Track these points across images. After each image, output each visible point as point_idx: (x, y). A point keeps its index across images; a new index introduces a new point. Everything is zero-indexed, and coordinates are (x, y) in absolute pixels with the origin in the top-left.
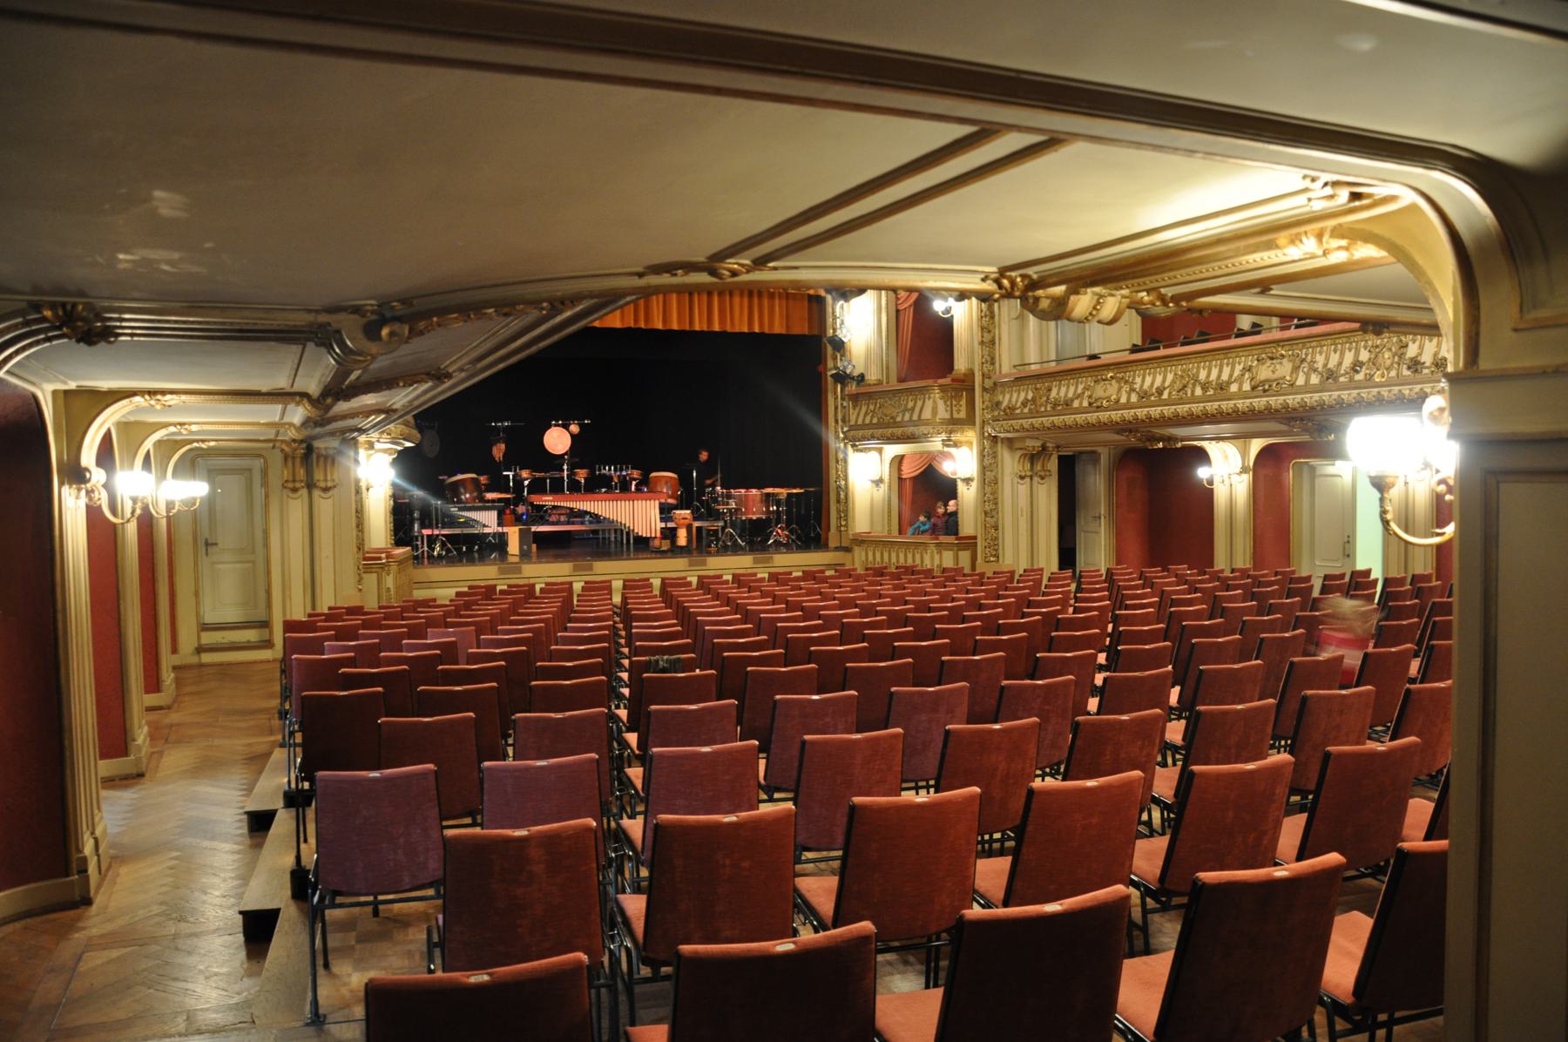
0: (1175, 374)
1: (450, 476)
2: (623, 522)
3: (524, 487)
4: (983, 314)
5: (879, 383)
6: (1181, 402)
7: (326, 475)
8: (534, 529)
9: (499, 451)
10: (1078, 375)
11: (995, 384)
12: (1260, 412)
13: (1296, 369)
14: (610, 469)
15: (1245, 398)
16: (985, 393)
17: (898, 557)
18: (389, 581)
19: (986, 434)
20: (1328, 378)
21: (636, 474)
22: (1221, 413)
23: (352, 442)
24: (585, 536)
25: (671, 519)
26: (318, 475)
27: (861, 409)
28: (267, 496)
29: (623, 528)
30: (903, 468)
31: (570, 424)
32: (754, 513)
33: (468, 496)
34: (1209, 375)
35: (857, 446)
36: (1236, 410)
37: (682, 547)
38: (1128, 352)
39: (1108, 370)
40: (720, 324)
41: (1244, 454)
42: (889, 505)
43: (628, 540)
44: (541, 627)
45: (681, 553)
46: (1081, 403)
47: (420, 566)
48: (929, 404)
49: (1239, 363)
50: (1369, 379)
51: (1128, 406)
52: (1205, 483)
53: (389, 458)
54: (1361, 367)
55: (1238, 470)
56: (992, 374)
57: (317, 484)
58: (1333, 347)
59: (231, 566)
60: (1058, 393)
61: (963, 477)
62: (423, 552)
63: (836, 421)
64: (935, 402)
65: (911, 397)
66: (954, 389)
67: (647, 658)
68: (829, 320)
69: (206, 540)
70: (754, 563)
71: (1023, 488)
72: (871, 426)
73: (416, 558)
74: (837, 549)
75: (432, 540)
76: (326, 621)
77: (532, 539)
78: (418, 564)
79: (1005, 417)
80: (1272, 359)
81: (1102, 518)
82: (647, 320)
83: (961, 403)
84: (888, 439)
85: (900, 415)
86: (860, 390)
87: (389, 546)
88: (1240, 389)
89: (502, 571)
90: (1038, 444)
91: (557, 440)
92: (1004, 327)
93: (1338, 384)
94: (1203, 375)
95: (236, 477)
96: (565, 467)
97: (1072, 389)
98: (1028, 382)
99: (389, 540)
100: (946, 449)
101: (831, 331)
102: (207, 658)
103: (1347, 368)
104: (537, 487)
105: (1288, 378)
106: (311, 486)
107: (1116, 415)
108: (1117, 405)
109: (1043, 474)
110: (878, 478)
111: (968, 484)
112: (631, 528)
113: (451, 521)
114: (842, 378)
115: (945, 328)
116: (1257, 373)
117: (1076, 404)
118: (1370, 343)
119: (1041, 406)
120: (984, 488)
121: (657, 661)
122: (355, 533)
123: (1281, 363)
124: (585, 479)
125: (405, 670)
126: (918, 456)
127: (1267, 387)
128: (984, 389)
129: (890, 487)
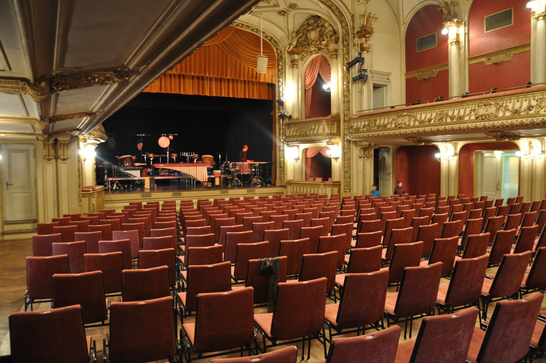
0: (437, 113)
1: (120, 156)
2: (192, 175)
3: (150, 161)
4: (344, 90)
5: (298, 119)
6: (440, 124)
7: (64, 152)
8: (156, 178)
9: (140, 146)
10: (389, 114)
11: (350, 119)
12: (480, 128)
13: (498, 110)
14: (186, 154)
15: (472, 123)
16: (345, 123)
17: (307, 190)
18: (94, 201)
19: (346, 139)
20: (515, 113)
21: (196, 156)
22: (460, 129)
23: (76, 138)
24: (175, 181)
25: (212, 174)
26: (60, 153)
27: (291, 130)
28: (36, 162)
29: (192, 178)
30: (307, 154)
31: (169, 136)
32: (246, 172)
33: (127, 164)
34: (453, 113)
35: (289, 144)
36: (468, 128)
37: (217, 186)
38: (405, 106)
39: (404, 112)
40: (232, 94)
41: (455, 147)
42: (302, 169)
43: (193, 182)
44: (173, 229)
45: (217, 188)
46: (391, 126)
47: (108, 194)
48: (321, 127)
49: (469, 108)
50: (537, 113)
51: (414, 127)
52: (438, 160)
53: (94, 147)
54: (533, 108)
55: (453, 154)
56: (348, 115)
57: (60, 157)
58: (517, 100)
59: (19, 195)
60: (380, 122)
61: (335, 157)
62: (109, 187)
63: (280, 135)
64: (324, 126)
65: (313, 124)
66: (332, 121)
67: (259, 260)
68: (277, 94)
69: (7, 182)
70: (247, 192)
71: (361, 162)
72: (296, 136)
73: (106, 190)
74: (280, 186)
75: (112, 183)
76: (60, 225)
77: (154, 182)
78: (107, 193)
79: (356, 132)
80: (485, 105)
81: (391, 174)
82: (203, 92)
83: (334, 127)
84: (304, 141)
85: (309, 132)
86: (290, 121)
87: (94, 185)
88: (470, 118)
89: (143, 196)
90: (367, 143)
91: (164, 142)
92: (354, 96)
93: (520, 116)
94: (450, 113)
95: (21, 154)
96: (168, 153)
97: (386, 120)
98: (365, 118)
99: (94, 183)
100: (328, 146)
101: (278, 98)
102: (7, 237)
103: (525, 108)
104: (156, 161)
105: (495, 113)
106: (57, 158)
107: (409, 131)
108: (409, 127)
109: (369, 156)
110: (297, 158)
111: (336, 160)
112: (196, 178)
113: (121, 175)
114: (283, 116)
115: (327, 96)
116: (478, 112)
117: (389, 126)
118: (537, 97)
119: (372, 127)
120: (345, 162)
121: (265, 262)
122: (77, 179)
123: (490, 107)
124: (176, 158)
125: (99, 273)
126: (314, 148)
127: (483, 118)
128: (345, 121)
129: (302, 161)
